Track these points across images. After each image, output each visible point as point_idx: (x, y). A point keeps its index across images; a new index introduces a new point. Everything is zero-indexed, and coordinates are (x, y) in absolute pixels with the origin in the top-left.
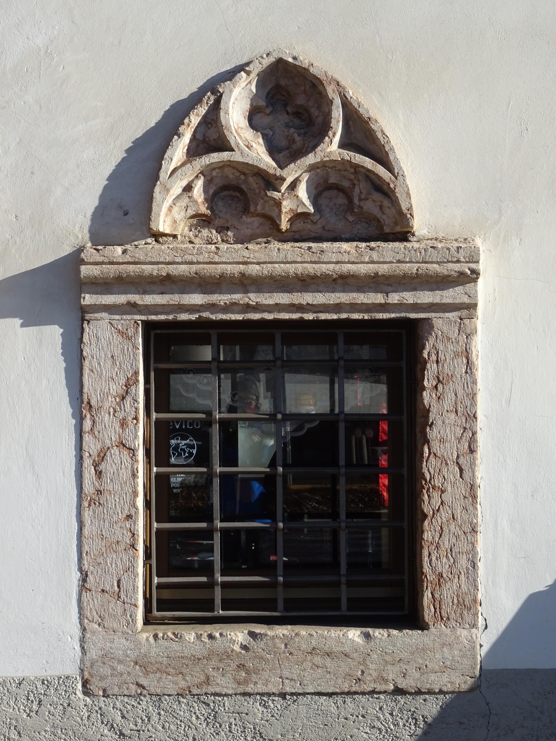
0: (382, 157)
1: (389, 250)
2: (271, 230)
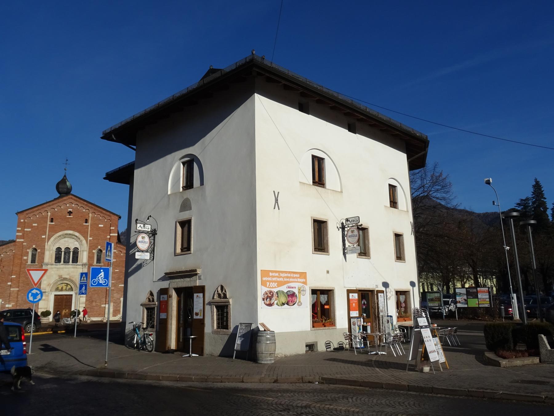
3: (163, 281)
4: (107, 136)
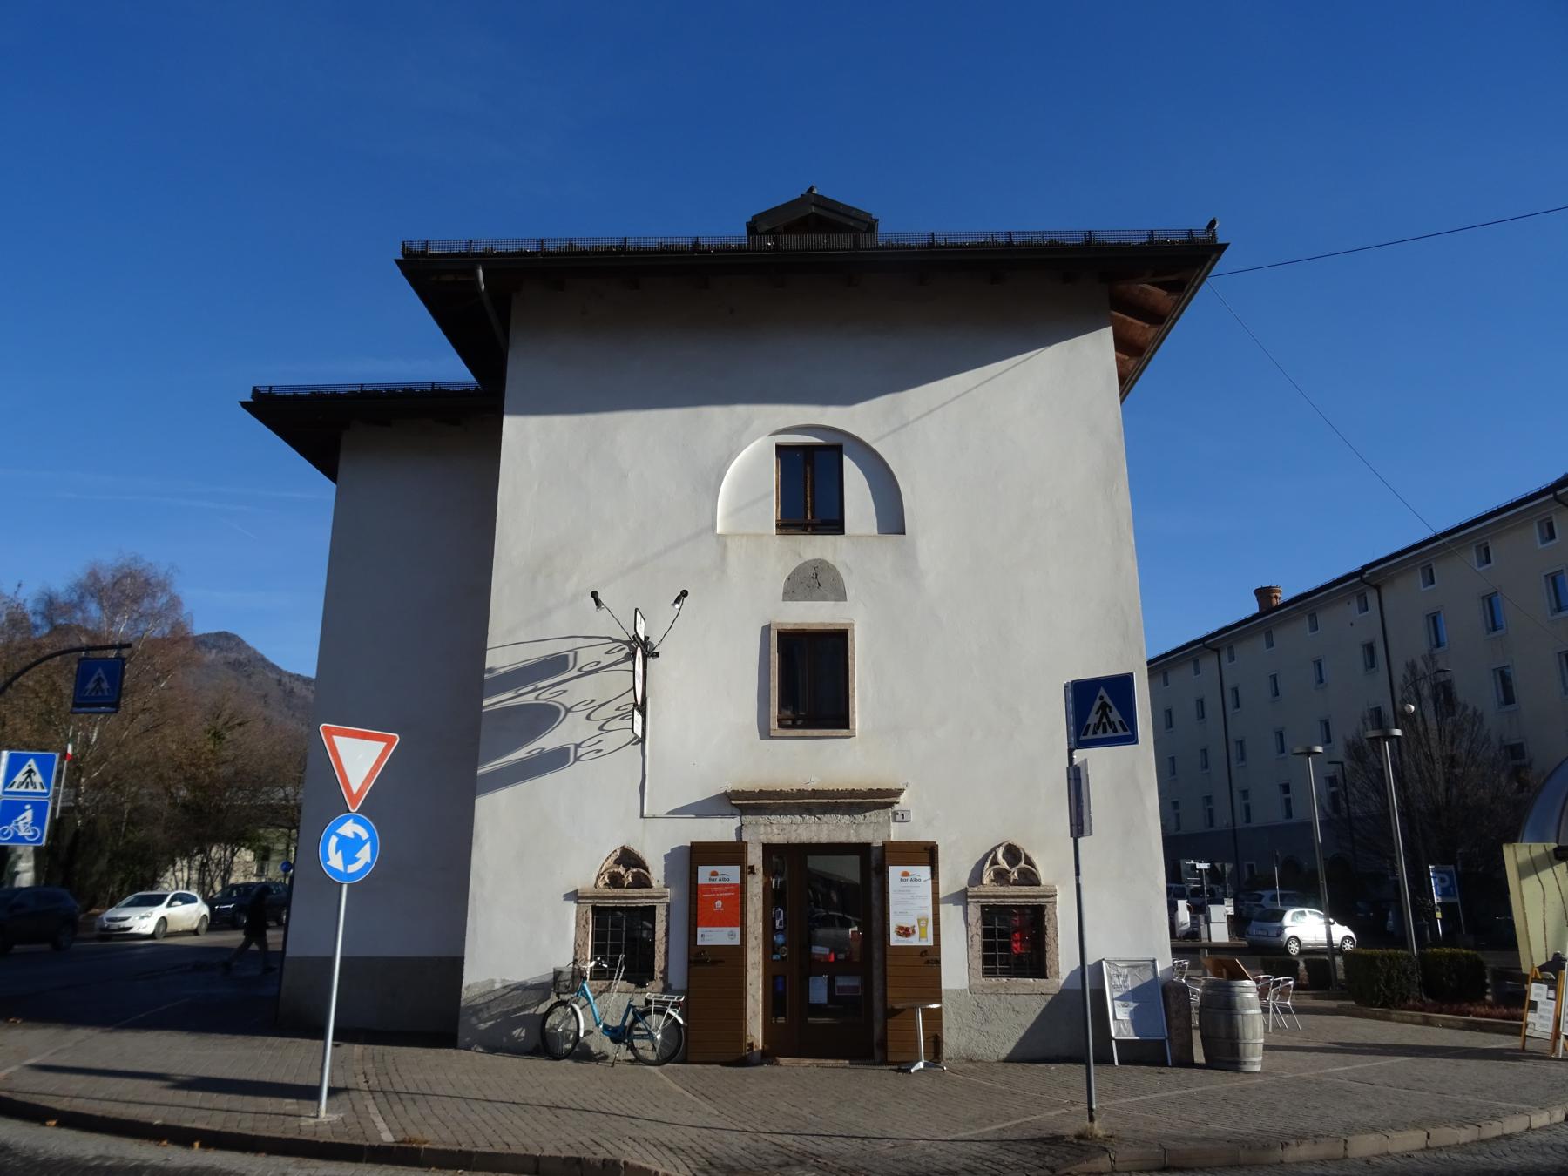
2: (1008, 883)
3: (698, 816)
4: (268, 407)
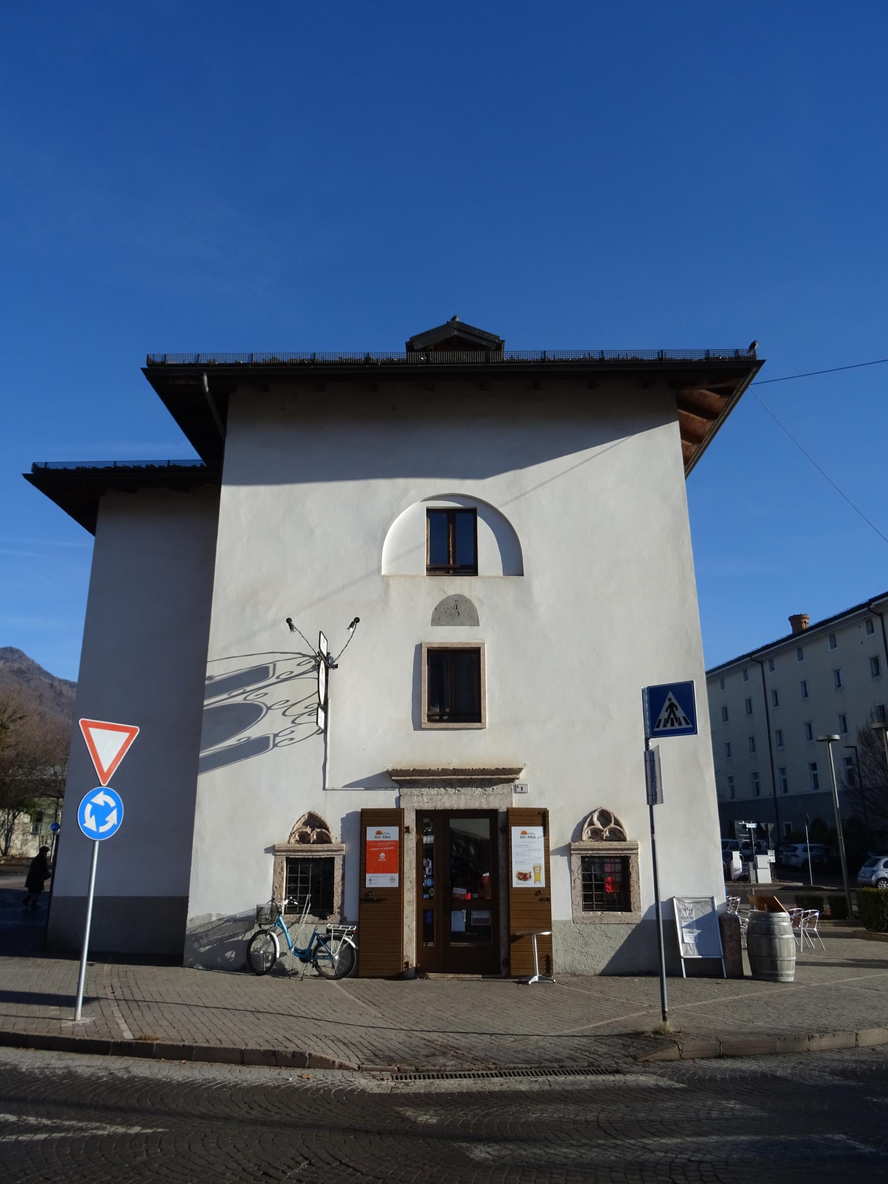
0: (621, 827)
1: (623, 843)
2: (602, 839)
3: (367, 789)
